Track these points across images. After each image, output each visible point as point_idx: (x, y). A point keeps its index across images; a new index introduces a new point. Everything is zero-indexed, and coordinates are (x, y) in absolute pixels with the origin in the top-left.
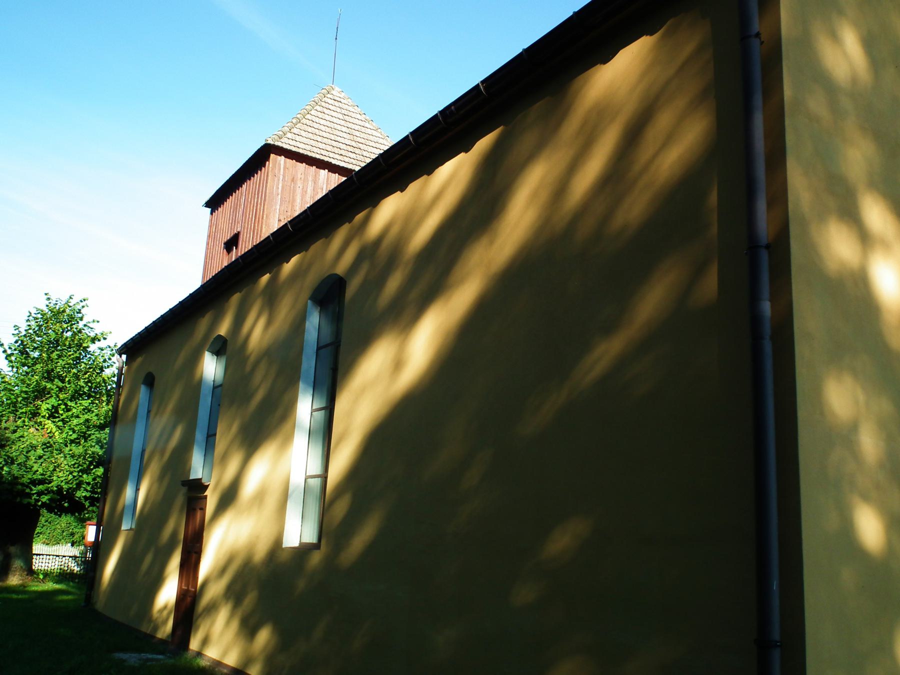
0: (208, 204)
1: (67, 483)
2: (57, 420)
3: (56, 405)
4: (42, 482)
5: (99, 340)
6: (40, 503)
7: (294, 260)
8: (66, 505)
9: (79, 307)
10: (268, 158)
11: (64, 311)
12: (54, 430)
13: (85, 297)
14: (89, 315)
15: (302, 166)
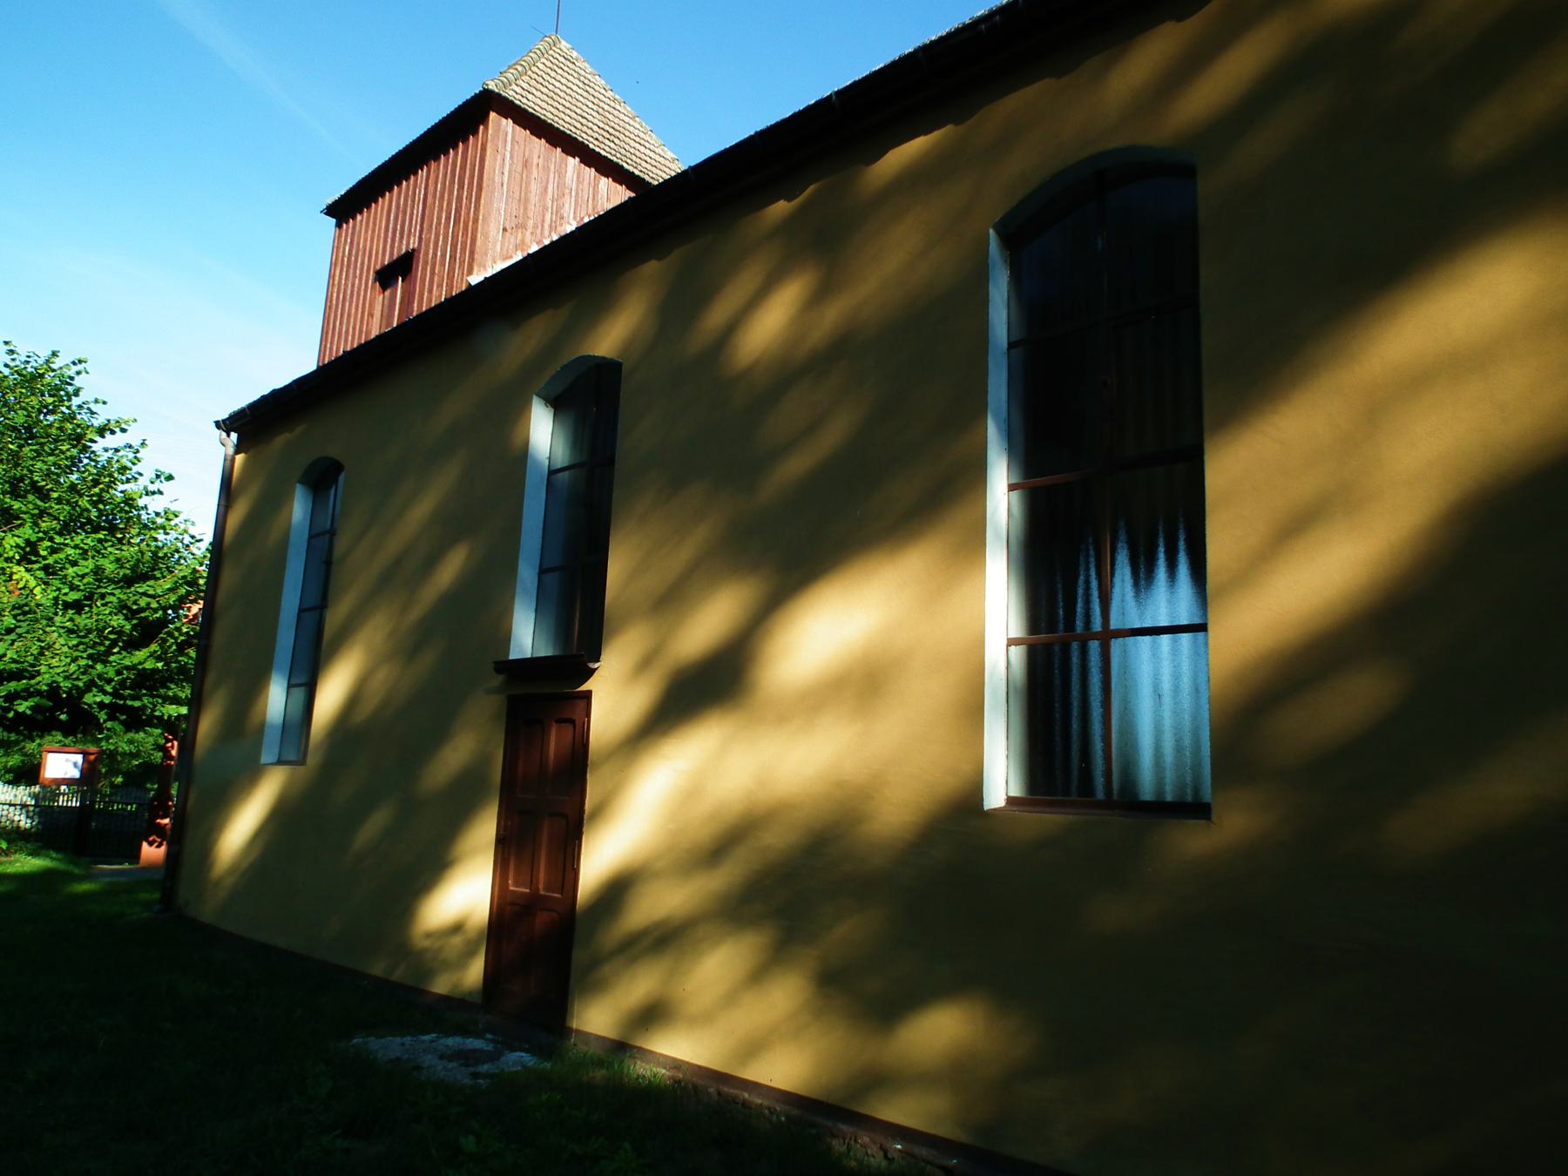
0: (331, 211)
1: (67, 678)
2: (36, 566)
3: (33, 539)
4: (17, 676)
5: (113, 432)
6: (11, 715)
7: (812, 188)
8: (63, 717)
9: (72, 373)
10: (484, 120)
11: (42, 376)
12: (32, 583)
13: (82, 357)
14: (89, 387)
15: (539, 145)
